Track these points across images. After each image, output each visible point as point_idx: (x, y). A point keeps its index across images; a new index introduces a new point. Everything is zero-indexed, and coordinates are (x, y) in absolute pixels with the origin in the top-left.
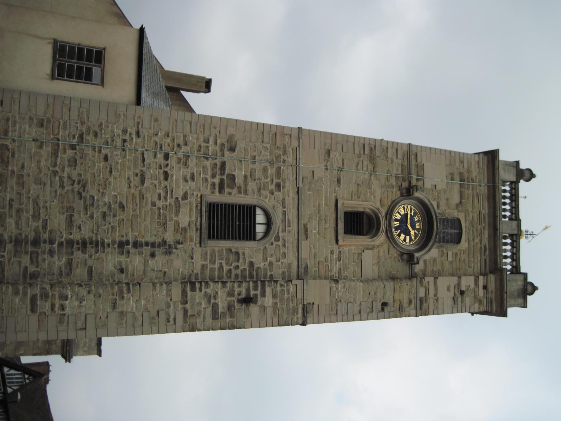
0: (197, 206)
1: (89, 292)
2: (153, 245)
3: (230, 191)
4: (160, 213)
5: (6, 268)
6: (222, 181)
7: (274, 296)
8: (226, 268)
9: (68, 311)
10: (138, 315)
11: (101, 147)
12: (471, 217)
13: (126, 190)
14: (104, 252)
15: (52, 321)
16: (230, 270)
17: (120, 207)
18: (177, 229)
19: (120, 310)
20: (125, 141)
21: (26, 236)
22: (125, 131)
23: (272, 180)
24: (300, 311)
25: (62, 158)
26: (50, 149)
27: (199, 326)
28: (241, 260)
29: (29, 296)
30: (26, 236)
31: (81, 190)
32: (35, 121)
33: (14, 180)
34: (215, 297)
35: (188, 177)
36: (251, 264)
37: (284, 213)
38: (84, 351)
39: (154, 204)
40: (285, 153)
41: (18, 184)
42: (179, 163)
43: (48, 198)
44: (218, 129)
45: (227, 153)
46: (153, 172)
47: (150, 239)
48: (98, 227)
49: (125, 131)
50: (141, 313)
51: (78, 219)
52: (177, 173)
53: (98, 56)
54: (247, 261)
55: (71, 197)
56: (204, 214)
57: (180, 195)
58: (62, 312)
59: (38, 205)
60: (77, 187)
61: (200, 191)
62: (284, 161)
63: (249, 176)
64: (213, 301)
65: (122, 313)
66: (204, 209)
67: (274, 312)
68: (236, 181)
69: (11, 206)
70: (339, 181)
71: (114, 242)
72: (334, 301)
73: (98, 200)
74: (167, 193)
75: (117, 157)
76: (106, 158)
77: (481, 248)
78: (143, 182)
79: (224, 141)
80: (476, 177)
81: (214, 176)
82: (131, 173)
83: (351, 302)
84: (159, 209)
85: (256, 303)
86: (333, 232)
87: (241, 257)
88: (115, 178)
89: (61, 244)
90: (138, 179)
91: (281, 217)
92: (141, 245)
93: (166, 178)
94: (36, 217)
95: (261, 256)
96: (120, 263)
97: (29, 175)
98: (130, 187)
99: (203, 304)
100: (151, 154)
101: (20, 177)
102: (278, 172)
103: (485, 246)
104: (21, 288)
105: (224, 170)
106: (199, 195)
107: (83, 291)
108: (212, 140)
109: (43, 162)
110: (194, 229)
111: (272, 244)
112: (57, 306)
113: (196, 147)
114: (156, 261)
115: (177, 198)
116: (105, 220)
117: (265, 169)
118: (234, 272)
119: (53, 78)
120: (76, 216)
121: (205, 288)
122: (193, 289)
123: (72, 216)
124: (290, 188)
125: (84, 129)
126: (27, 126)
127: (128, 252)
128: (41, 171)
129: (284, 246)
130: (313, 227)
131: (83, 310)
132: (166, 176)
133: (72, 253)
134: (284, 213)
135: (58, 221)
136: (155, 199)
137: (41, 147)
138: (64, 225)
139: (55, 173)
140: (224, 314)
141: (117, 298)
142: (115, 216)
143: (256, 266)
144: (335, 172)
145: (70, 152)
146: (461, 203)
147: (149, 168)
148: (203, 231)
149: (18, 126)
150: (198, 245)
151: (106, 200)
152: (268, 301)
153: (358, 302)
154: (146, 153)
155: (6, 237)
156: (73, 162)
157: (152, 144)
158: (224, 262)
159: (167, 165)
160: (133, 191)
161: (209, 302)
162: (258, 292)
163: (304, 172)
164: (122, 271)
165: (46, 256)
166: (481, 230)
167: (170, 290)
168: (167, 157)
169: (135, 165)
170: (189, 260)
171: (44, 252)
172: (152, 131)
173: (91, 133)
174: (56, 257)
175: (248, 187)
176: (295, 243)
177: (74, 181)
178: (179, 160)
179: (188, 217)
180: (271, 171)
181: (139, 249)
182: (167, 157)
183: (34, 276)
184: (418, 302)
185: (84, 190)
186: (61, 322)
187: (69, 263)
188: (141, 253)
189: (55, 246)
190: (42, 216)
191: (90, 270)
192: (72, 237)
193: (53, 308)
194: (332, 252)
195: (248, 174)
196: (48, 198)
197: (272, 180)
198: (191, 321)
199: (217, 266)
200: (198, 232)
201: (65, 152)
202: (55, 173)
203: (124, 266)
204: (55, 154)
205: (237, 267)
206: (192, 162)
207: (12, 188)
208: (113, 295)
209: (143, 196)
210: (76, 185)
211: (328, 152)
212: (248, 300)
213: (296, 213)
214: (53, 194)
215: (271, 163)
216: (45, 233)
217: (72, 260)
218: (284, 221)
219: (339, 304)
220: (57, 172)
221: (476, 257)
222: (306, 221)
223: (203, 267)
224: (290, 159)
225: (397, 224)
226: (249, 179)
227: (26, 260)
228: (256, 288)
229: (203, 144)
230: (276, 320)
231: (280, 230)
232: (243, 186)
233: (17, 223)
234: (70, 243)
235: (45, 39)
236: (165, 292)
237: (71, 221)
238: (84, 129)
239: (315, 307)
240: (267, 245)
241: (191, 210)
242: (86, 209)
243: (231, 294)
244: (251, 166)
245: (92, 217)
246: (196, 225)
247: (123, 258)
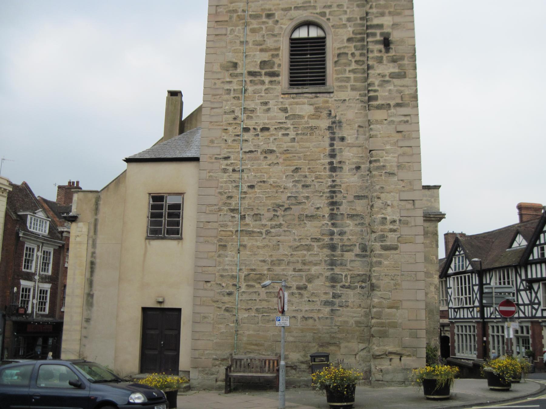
0: (293, 98)
1: (379, 198)
2: (333, 139)
3: (276, 65)
4: (301, 134)
5: (356, 272)
6: (267, 74)
7: (382, 15)
8: (354, 66)
9: (396, 218)
10: (400, 151)
11: (241, 192)
13: (280, 168)
14: (340, 185)
15: (405, 231)
16: (356, 61)
20: (234, 170)
22: (225, 171)
23: (264, 23)
26: (246, 238)
28: (346, 51)
29: (383, 252)
31: (283, 208)
34: (383, 76)
36: (349, 40)
38: (435, 202)
40: (235, 11)
41: (279, 265)
42: (252, 117)
44: (217, 81)
45: (239, 71)
47: (327, 142)
48: (316, 191)
49: (225, 171)
50: (399, 149)
51: (309, 209)
52: (261, 118)
53: (157, 199)
54: (346, 44)
56: (300, 91)
57: (283, 115)
58: (398, 222)
61: (278, 96)
62: (244, 11)
63: (261, 47)
64: (387, 78)
66: (295, 91)
67: (399, 14)
68: (266, 59)
69: (300, 270)
71: (331, 176)
75: (249, 177)
76: (252, 187)
78: (272, 152)
79: (227, 74)
81: (263, 83)
84: (297, 134)
85: (389, 34)
87: (342, 51)
88: (270, 177)
91: (300, 12)
92: (333, 150)
93: (268, 129)
94: (309, 248)
96: (351, 170)
98: (278, 163)
99: (390, 88)
100: (245, 144)
101: (273, 263)
102: (256, 17)
104: (375, 260)
105: (256, 72)
106: (282, 96)
107: (378, 204)
108: (227, 87)
109: (259, 244)
113: (235, 102)
114: (348, 135)
115: (286, 118)
116: (310, 185)
117: (253, 31)
118: (358, 58)
119: (181, 239)
120: (307, 212)
121: (375, 86)
122: (375, 98)
123: (307, 216)
125: (226, 208)
126: (226, 259)
127: (340, 162)
129: (330, 7)
131: (395, 203)
132: (264, 129)
133: (342, 214)
135: (312, 229)
137: (245, 246)
138: (316, 223)
139: (268, 233)
140: (400, 66)
141: (384, 172)
142: (306, 177)
145: (248, 220)
149: (227, 267)
150: (332, 95)
151: (290, 185)
152: (387, 21)
154: (244, 150)
158: (348, 69)
159: (254, 129)
160: (281, 160)
161: (388, 82)
162: (378, 32)
164: (358, 168)
165: (345, 238)
167: (377, 121)
168: (246, 130)
172: (223, 145)
173: (228, 201)
174: (346, 229)
175: (272, 47)
178: (249, 117)
179: (304, 105)
180: (255, 24)
181: (337, 152)
182: (246, 130)
183: (364, 248)
186: (406, 223)
187: (351, 216)
188: (341, 150)
189: (335, 230)
191: (358, 197)
192: (327, 215)
193: (392, 231)
195: (259, 47)
197: (264, 23)
198: (407, 100)
199: (352, 75)
200: (318, 95)
202: (268, 233)
203: (354, 166)
205: (353, 54)
207: (283, 270)
208: (381, 175)
209: (285, 151)
210: (278, 214)
212: (387, 43)
216: (324, 240)
217: (348, 215)
223: (353, 89)
226: (264, 47)
227: (349, 256)
228: (374, 35)
229: (232, 95)
230: (407, 12)
231: (315, 11)
233: (316, 265)
234: (332, 216)
235: (146, 247)
236: (378, 126)
238: (226, 208)
240: (330, 24)
241: (297, 104)
242: (300, 203)
243: (380, 60)
244: (250, 45)
245: (307, 198)
246: (312, 98)
247: (346, 168)
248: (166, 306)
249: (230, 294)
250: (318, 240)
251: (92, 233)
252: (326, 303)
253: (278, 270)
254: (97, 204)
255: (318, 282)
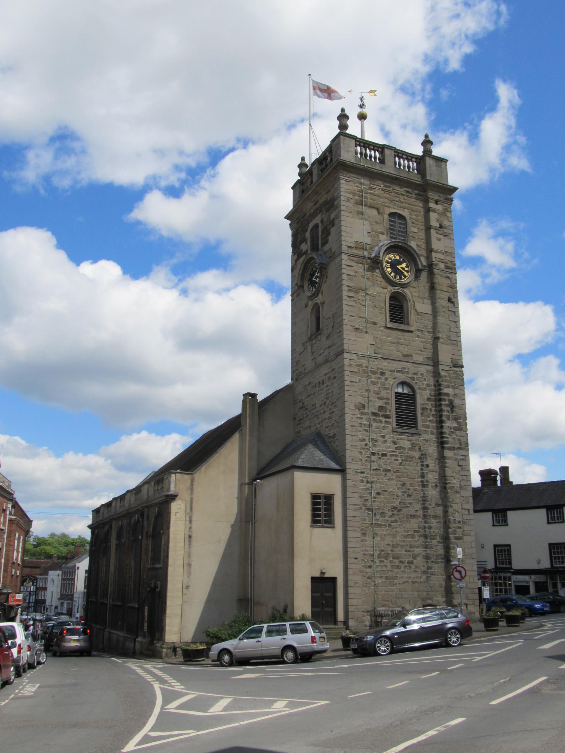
2: (422, 465)
7: (448, 387)
12: (386, 201)
17: (404, 486)
18: (412, 449)
19: (459, 489)
20: (367, 482)
21: (423, 542)
24: (455, 369)
25: (381, 522)
27: (465, 440)
30: (423, 542)
31: (397, 510)
32: (363, 538)
33: (395, 549)
35: (384, 439)
36: (428, 399)
37: (398, 371)
39: (401, 464)
41: (397, 547)
43: (402, 529)
44: (353, 416)
46: (383, 463)
47: (419, 468)
49: (362, 481)
51: (412, 512)
52: (381, 447)
55: (402, 516)
57: (393, 446)
59: (407, 536)
60: (395, 512)
65: (461, 488)
66: (401, 430)
67: (457, 388)
69: (409, 551)
70: (375, 323)
71: (422, 490)
72: (449, 342)
73: (401, 500)
74: (394, 455)
75: (377, 487)
77: (407, 196)
80: (357, 186)
81: (381, 422)
82: (385, 478)
83: (450, 328)
84: (403, 460)
86: (406, 334)
87: (425, 406)
89: (426, 522)
90: (388, 474)
92: (423, 473)
94: (413, 537)
95: (424, 392)
96: (432, 487)
97: (392, 541)
101: (394, 546)
102: (374, 373)
103: (407, 192)
108: (360, 421)
109: (384, 533)
110: (412, 438)
111: (416, 383)
112: (459, 525)
113: (365, 433)
115: (396, 448)
117: (373, 383)
120: (410, 513)
123: (411, 516)
124: (384, 364)
128: (390, 534)
130: (405, 350)
132: (384, 455)
134: (398, 371)
135: (414, 524)
136: (397, 462)
137: (377, 534)
142: (409, 489)
143: (429, 397)
144: (368, 325)
145: (377, 517)
146: (377, 209)
147: (381, 466)
148: (413, 432)
149: (368, 548)
151: (400, 494)
152: (450, 391)
153: (449, 322)
154: (373, 468)
155: (424, 553)
156: (383, 514)
157: (367, 463)
158: (429, 419)
160: (394, 477)
161: (453, 432)
163: (370, 351)
164: (436, 486)
165: (432, 531)
166: (395, 193)
168: (373, 454)
169: (380, 475)
170: (428, 443)
171: (430, 532)
172: (360, 463)
174: (432, 525)
176: (415, 365)
177: (393, 514)
178: (374, 445)
181: (425, 474)
182: (373, 454)
184: (448, 270)
185: (397, 508)
186: (466, 523)
189: (426, 525)
190: (412, 533)
193: (460, 528)
194: (418, 337)
195: (377, 396)
196: (402, 529)
197: (379, 378)
199: (431, 424)
201: (378, 520)
202: (390, 526)
203: (434, 485)
204: (380, 526)
205: (431, 409)
206: (374, 436)
207: (400, 550)
211: (357, 329)
213: (397, 362)
214: (401, 526)
215: (368, 377)
218: (402, 372)
219: (452, 338)
220: (389, 524)
221: (414, 203)
222: (400, 354)
224: (364, 361)
225: (398, 277)
226: (380, 396)
227: (434, 542)
232: (384, 401)
234: (425, 516)
237: (414, 516)
238: (364, 508)
239: (454, 357)
240: (417, 387)
241: (401, 439)
242: (407, 507)
244: (372, 393)
245: (410, 503)
247: (430, 485)
248: (326, 575)
249: (370, 567)
250: (418, 532)
251: (189, 510)
252: (424, 572)
253: (397, 550)
254: (192, 485)
255: (420, 559)
